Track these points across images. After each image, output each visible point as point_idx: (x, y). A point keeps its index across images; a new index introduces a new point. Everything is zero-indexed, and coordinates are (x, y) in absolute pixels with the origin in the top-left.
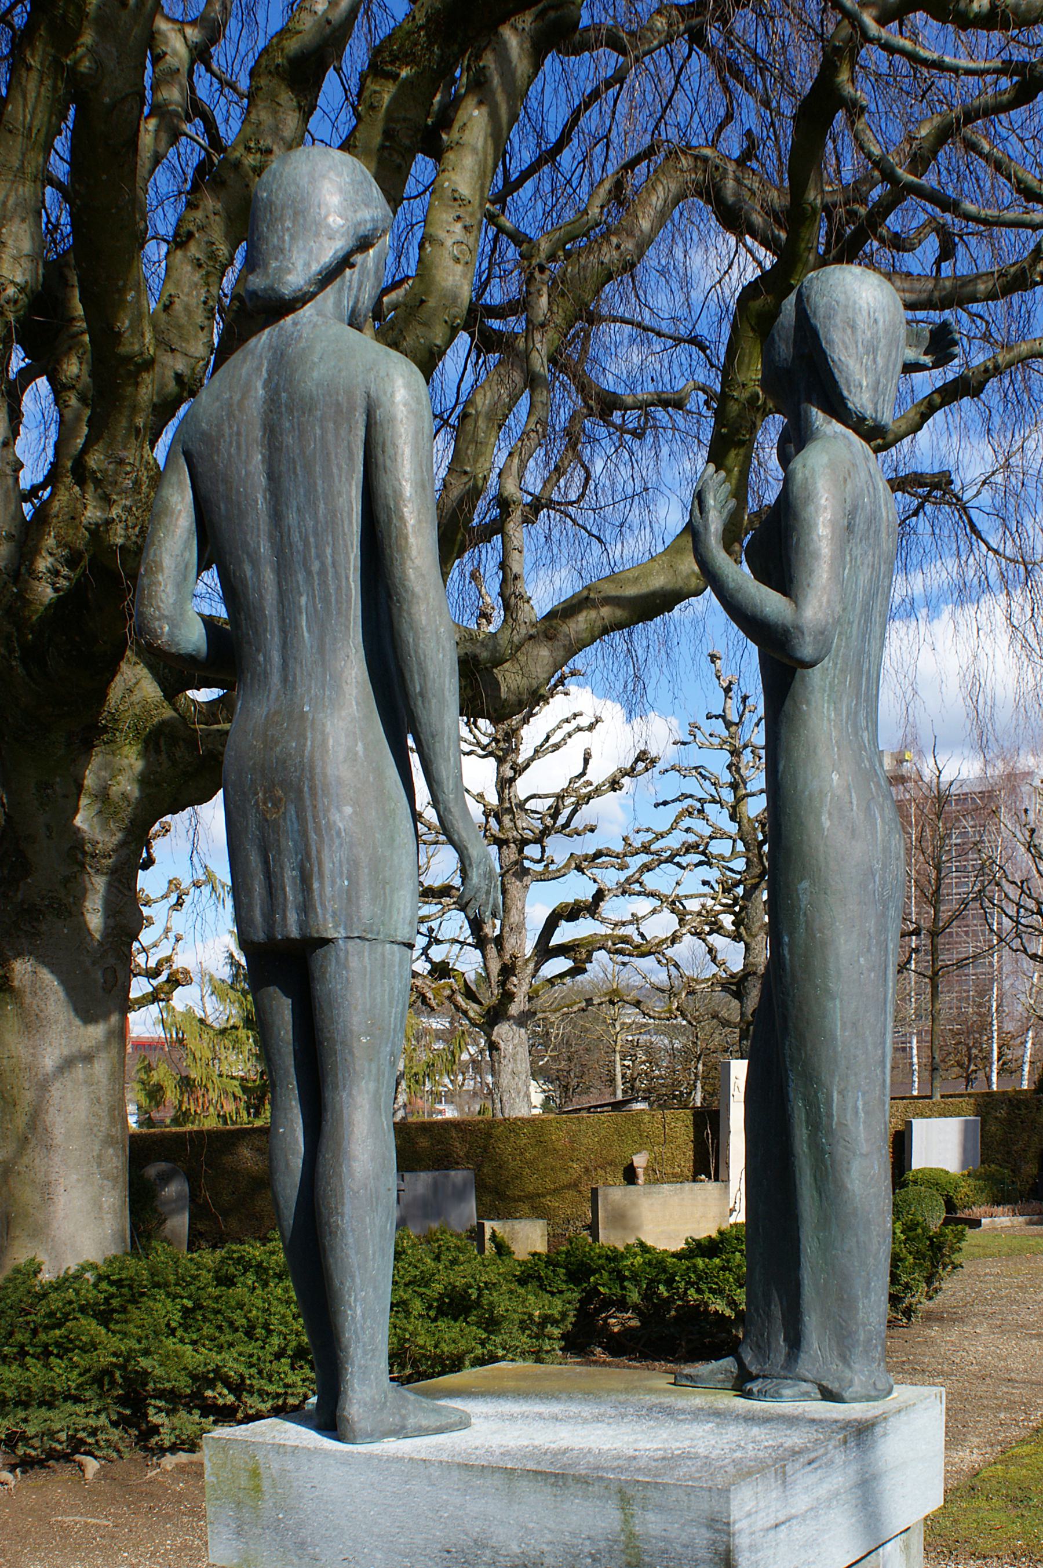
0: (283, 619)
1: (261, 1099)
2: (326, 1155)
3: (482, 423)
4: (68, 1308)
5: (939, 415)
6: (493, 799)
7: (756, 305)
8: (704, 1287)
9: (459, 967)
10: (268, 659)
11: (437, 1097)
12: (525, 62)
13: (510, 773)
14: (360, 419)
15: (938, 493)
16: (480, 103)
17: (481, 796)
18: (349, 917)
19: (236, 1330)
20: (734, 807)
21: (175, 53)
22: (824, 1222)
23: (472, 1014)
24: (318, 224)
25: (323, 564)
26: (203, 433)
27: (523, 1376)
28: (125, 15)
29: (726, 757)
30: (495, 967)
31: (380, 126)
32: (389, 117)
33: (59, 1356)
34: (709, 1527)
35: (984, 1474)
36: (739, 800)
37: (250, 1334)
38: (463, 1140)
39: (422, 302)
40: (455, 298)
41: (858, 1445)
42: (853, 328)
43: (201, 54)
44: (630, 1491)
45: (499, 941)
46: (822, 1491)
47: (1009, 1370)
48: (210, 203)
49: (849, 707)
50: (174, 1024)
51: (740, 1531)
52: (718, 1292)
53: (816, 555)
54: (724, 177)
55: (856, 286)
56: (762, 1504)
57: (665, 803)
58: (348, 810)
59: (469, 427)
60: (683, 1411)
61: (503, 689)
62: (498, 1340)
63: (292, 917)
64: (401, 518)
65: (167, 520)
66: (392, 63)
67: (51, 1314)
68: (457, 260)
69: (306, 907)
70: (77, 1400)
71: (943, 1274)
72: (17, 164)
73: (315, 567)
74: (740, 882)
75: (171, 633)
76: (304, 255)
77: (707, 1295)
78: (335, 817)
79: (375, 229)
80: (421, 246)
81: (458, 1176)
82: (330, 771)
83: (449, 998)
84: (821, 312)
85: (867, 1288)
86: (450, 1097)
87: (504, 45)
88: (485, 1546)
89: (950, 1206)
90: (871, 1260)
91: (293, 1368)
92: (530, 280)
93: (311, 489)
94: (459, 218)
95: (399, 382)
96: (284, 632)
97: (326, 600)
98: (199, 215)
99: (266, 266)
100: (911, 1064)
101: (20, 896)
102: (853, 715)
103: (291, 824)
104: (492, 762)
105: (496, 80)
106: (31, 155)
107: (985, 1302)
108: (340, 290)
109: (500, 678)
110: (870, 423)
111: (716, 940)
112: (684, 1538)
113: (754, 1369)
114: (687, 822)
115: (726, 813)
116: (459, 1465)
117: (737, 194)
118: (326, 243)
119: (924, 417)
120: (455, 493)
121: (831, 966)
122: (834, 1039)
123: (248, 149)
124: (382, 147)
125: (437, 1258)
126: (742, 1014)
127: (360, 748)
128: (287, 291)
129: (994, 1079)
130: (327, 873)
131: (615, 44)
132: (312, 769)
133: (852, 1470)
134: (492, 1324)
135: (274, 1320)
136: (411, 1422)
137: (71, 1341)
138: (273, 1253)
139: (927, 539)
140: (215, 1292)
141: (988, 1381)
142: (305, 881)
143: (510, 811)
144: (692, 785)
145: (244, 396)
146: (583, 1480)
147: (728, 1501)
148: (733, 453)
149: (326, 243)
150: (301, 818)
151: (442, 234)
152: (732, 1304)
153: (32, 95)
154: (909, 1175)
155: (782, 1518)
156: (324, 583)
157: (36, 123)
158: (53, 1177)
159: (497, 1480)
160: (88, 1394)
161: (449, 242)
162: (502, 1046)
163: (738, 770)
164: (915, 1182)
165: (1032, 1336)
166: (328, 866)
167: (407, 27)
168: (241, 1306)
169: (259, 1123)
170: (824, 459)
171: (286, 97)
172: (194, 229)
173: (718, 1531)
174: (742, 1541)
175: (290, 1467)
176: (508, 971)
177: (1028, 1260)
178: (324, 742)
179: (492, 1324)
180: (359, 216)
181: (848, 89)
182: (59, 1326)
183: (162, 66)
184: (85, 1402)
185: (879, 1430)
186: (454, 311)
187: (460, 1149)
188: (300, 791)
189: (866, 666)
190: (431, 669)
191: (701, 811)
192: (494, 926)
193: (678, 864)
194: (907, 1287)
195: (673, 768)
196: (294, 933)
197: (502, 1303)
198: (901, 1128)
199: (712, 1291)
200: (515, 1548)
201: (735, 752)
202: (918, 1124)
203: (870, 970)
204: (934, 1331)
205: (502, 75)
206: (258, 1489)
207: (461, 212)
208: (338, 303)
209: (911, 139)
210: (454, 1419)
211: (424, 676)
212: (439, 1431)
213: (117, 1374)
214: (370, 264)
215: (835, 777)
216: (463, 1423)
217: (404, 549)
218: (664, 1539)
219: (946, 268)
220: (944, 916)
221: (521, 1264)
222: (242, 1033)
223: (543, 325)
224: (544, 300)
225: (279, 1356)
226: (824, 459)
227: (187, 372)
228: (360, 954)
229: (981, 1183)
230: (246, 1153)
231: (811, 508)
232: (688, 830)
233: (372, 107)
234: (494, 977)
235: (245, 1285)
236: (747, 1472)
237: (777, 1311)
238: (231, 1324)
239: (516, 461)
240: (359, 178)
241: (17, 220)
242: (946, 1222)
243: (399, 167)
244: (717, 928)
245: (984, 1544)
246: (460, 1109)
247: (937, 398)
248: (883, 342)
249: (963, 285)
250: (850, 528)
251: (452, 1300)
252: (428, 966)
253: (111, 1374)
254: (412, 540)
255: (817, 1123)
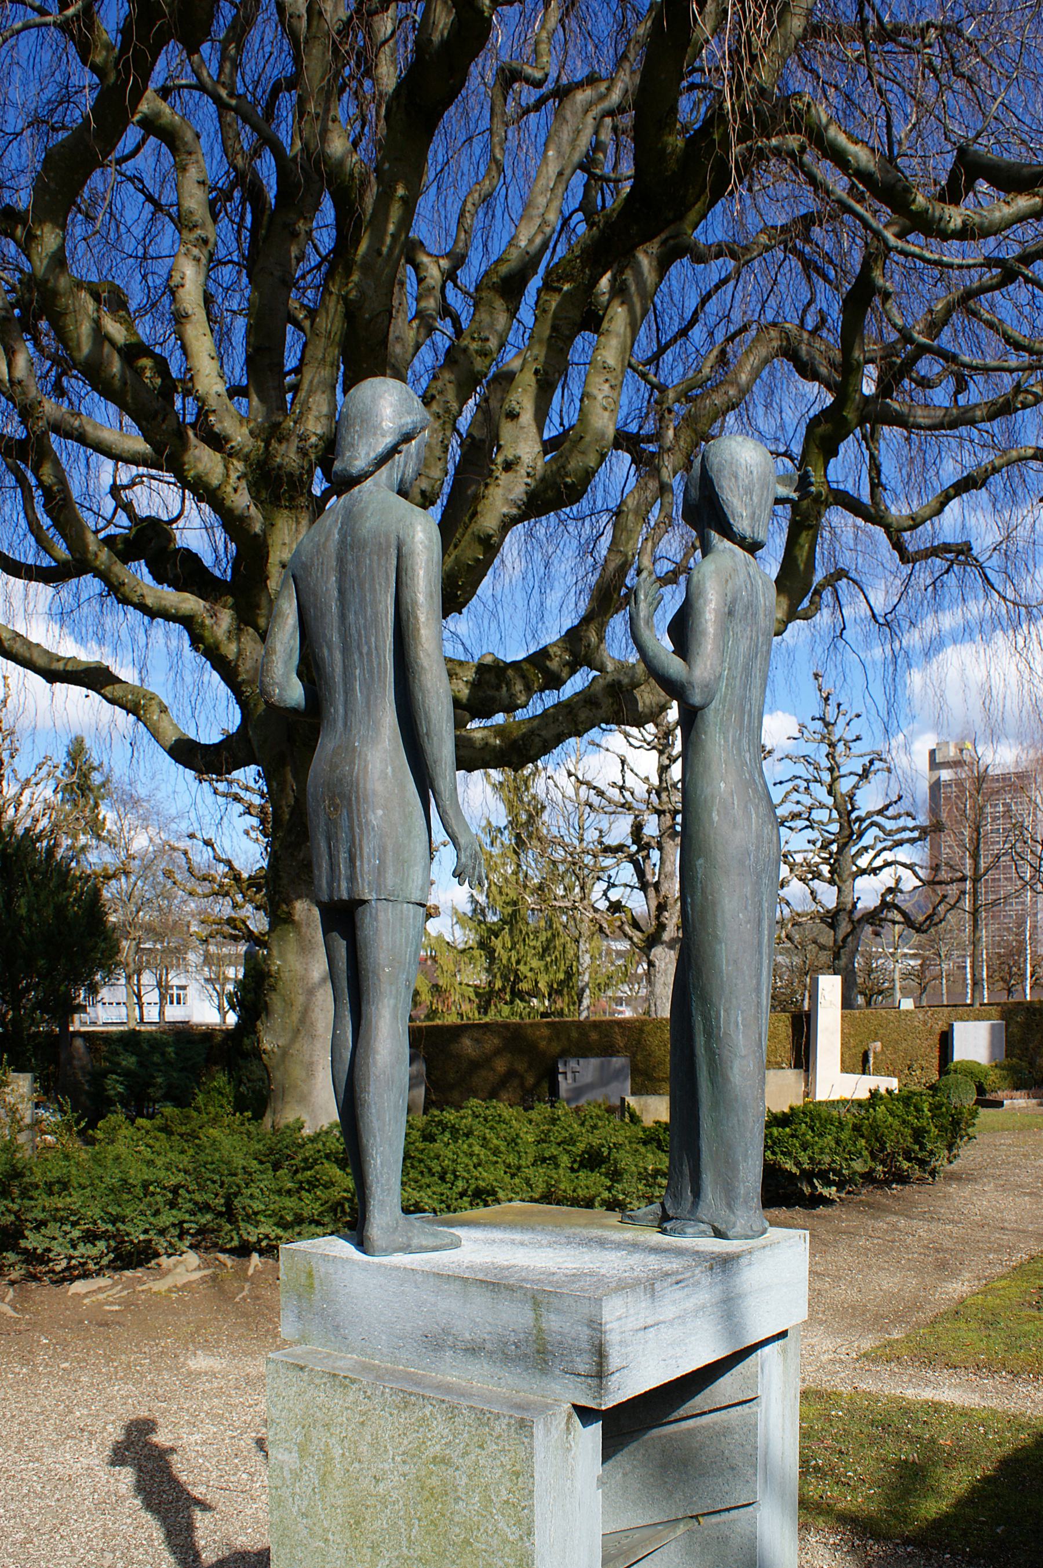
0: (345, 684)
1: (488, 1003)
2: (360, 1051)
3: (631, 517)
4: (317, 1155)
5: (954, 503)
6: (655, 781)
7: (820, 430)
8: (777, 1150)
9: (630, 905)
10: (337, 711)
11: (619, 1001)
12: (653, 274)
13: (667, 762)
14: (393, 552)
15: (962, 558)
16: (623, 303)
17: (647, 778)
18: (379, 885)
19: (433, 1175)
20: (830, 786)
21: (432, 277)
22: (716, 1105)
23: (635, 940)
24: (375, 427)
25: (369, 648)
26: (303, 563)
27: (522, 1213)
28: (380, 260)
29: (825, 749)
30: (654, 904)
31: (549, 323)
32: (555, 316)
33: (308, 1191)
34: (589, 1326)
35: (969, 1302)
36: (834, 780)
37: (442, 1178)
38: (623, 1035)
39: (582, 437)
40: (603, 435)
41: (723, 1271)
42: (736, 477)
43: (450, 276)
44: (540, 1298)
45: (657, 886)
46: (690, 1304)
47: (1003, 1220)
48: (447, 376)
49: (734, 736)
50: (430, 945)
51: (611, 1331)
52: (787, 1154)
53: (704, 633)
54: (801, 342)
55: (738, 449)
56: (632, 1311)
57: (781, 783)
58: (380, 812)
59: (622, 520)
60: (612, 1242)
61: (640, 704)
62: (619, 1186)
63: (344, 885)
64: (416, 618)
65: (279, 620)
66: (558, 281)
67: (305, 1160)
68: (605, 409)
69: (352, 879)
70: (318, 1223)
71: (961, 1143)
72: (320, 356)
73: (365, 650)
74: (834, 841)
75: (280, 694)
76: (366, 448)
77: (780, 1156)
78: (371, 817)
79: (415, 428)
80: (581, 400)
81: (618, 1062)
82: (369, 786)
83: (619, 927)
84: (715, 467)
85: (746, 1156)
86: (628, 1001)
87: (638, 264)
88: (449, 1334)
89: (981, 1090)
90: (748, 1134)
91: (471, 1205)
92: (662, 418)
93: (363, 599)
94: (607, 380)
95: (419, 528)
96: (346, 692)
97: (371, 672)
98: (439, 383)
99: (343, 455)
100: (965, 979)
101: (302, 855)
102: (738, 741)
103: (344, 823)
104: (655, 753)
105: (633, 288)
106: (330, 350)
107: (996, 1166)
108: (391, 468)
109: (638, 697)
110: (749, 540)
111: (816, 884)
112: (573, 1334)
113: (671, 1213)
114: (795, 796)
115: (825, 789)
116: (435, 1274)
117: (808, 353)
118: (380, 439)
119: (943, 505)
120: (612, 566)
121: (719, 919)
122: (721, 972)
123: (473, 339)
124: (551, 337)
125: (582, 1124)
126: (835, 941)
127: (389, 770)
128: (354, 471)
129: (1028, 991)
130: (365, 855)
131: (733, 256)
132: (358, 785)
133: (717, 1290)
134: (616, 1175)
135: (459, 1168)
136: (415, 1242)
137: (318, 1180)
138: (462, 1118)
139: (955, 591)
140: (420, 1145)
141: (986, 1228)
142: (352, 860)
143: (666, 789)
144: (801, 770)
145: (327, 540)
146: (510, 1288)
147: (601, 1308)
148: (804, 534)
149: (380, 439)
150: (351, 819)
151: (595, 392)
152: (798, 1164)
153: (332, 311)
154: (951, 1066)
155: (650, 1322)
156: (370, 661)
157: (334, 329)
158: (315, 1058)
159: (456, 1286)
160: (326, 1220)
161: (600, 397)
162: (657, 963)
163: (834, 758)
164: (955, 1071)
165: (1026, 1194)
166: (366, 850)
167: (568, 257)
168: (438, 1157)
169: (486, 1019)
170: (713, 567)
171: (499, 304)
172: (435, 392)
173: (594, 1329)
174: (613, 1338)
175: (332, 1271)
176: (661, 908)
177: (1035, 1134)
178: (366, 767)
179: (616, 1175)
180: (403, 421)
181: (880, 281)
182: (310, 1168)
183: (424, 285)
184: (323, 1225)
185: (744, 1261)
186: (604, 443)
187: (620, 1041)
188: (350, 799)
189: (748, 707)
190: (434, 717)
191: (807, 788)
192: (654, 874)
193: (790, 828)
194: (932, 1153)
195: (787, 757)
196: (345, 896)
197: (625, 1160)
198: (945, 1029)
199: (783, 1153)
200: (467, 1336)
201: (832, 745)
202: (958, 1026)
203: (749, 922)
204: (953, 1188)
205: (637, 284)
206: (311, 1286)
207: (608, 376)
208: (390, 476)
209: (931, 311)
210: (447, 1241)
211: (429, 722)
212: (435, 1249)
213: (347, 1205)
214: (413, 450)
215: (722, 785)
216: (456, 1244)
217: (416, 637)
218: (561, 1334)
219: (962, 400)
220: (982, 865)
221: (644, 1130)
222: (477, 953)
223: (669, 450)
224: (671, 433)
225: (462, 1195)
226: (713, 567)
227: (429, 489)
228: (386, 910)
229: (1005, 1072)
230: (467, 1042)
231: (701, 601)
232: (798, 803)
233: (545, 311)
234: (653, 913)
235: (442, 1141)
236: (622, 1286)
237: (686, 1170)
238: (430, 1170)
239: (650, 544)
240: (405, 396)
241: (319, 393)
242: (978, 1102)
243: (562, 349)
244: (818, 876)
245: (956, 1357)
246: (635, 1010)
247: (952, 492)
248: (757, 486)
249: (966, 412)
250: (730, 613)
251: (590, 1156)
252: (607, 904)
253: (342, 1205)
254: (422, 632)
255: (710, 1034)
